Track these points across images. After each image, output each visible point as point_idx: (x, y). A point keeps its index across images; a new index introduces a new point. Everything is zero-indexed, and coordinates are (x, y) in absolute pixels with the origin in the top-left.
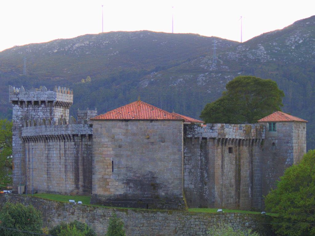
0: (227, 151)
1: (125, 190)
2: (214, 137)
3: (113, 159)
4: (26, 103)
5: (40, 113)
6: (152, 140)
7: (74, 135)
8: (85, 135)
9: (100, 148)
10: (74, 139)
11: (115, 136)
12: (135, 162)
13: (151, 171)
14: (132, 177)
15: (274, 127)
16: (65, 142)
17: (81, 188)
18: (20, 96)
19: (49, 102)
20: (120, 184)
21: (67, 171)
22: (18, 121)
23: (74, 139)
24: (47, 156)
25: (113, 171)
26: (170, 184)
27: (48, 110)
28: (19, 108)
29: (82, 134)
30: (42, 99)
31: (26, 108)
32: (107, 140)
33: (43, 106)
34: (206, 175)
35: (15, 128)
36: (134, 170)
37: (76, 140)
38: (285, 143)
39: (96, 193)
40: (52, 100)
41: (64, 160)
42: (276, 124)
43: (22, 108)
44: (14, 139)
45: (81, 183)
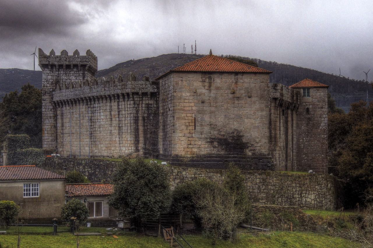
1: (208, 150)
2: (276, 97)
3: (195, 115)
4: (57, 67)
5: (72, 77)
6: (237, 95)
7: (133, 94)
9: (181, 103)
10: (133, 98)
11: (198, 90)
12: (219, 119)
13: (237, 129)
14: (216, 136)
15: (308, 93)
16: (118, 102)
17: (141, 150)
19: (82, 66)
20: (204, 143)
21: (122, 133)
22: (48, 85)
23: (133, 98)
24: (91, 119)
25: (195, 129)
26: (257, 143)
27: (80, 74)
29: (143, 92)
31: (57, 72)
32: (188, 94)
33: (75, 70)
35: (45, 93)
36: (219, 128)
37: (136, 99)
38: (319, 108)
39: (177, 153)
40: (85, 64)
41: (117, 121)
45: (141, 145)
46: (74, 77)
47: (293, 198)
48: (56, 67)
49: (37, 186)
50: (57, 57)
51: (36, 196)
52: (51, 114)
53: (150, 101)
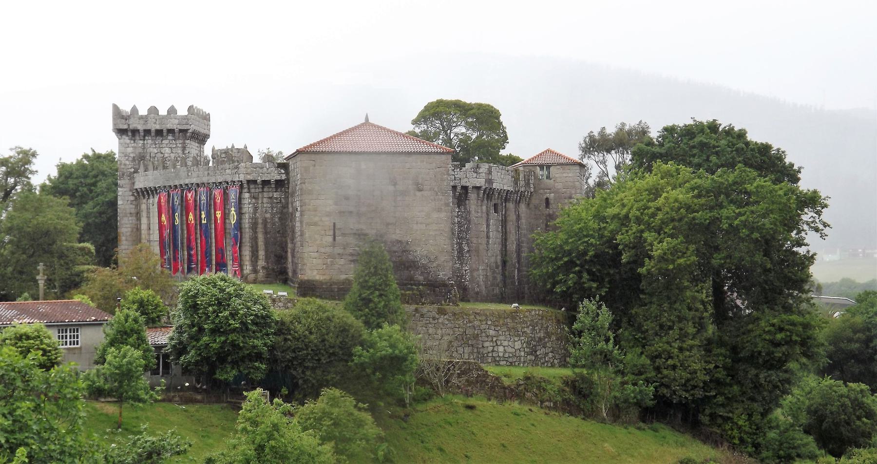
0: (492, 208)
4: (142, 134)
8: (270, 181)
9: (312, 201)
13: (400, 239)
17: (261, 271)
18: (131, 121)
19: (181, 131)
22: (127, 162)
23: (249, 189)
28: (128, 141)
30: (170, 126)
31: (141, 142)
33: (170, 137)
34: (466, 248)
35: (123, 175)
42: (551, 169)
43: (134, 140)
44: (120, 193)
45: (261, 263)
46: (168, 149)
47: (483, 347)
48: (139, 133)
49: (77, 332)
50: (142, 117)
51: (76, 346)
52: (131, 208)
53: (275, 194)
